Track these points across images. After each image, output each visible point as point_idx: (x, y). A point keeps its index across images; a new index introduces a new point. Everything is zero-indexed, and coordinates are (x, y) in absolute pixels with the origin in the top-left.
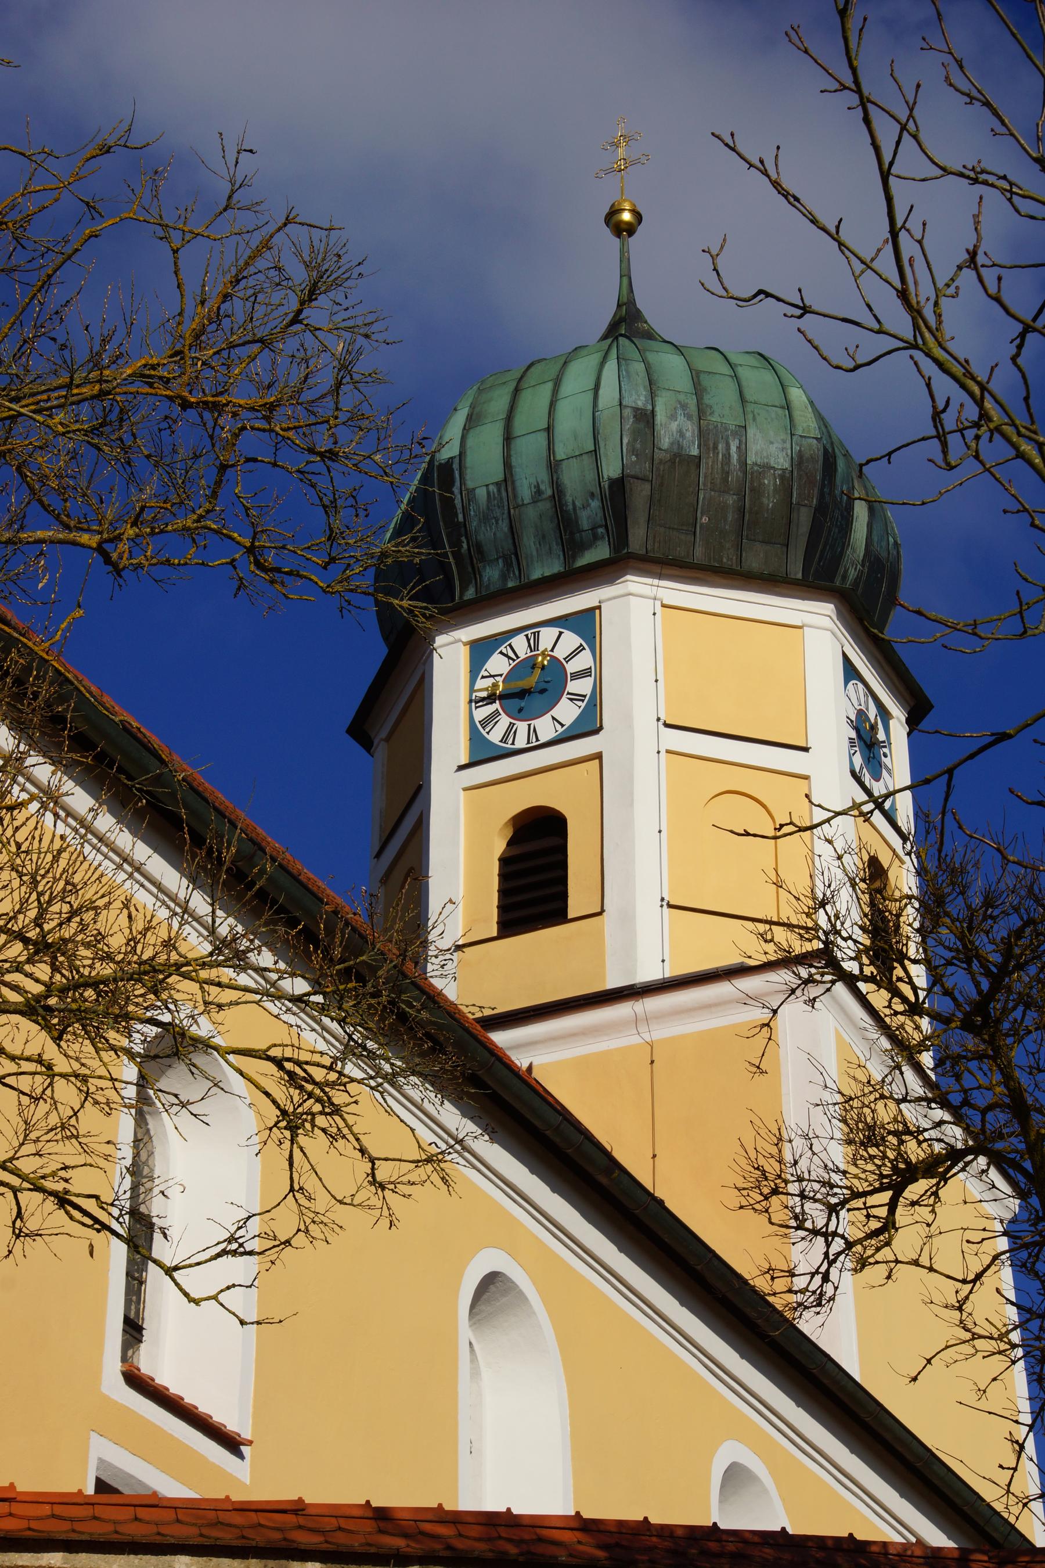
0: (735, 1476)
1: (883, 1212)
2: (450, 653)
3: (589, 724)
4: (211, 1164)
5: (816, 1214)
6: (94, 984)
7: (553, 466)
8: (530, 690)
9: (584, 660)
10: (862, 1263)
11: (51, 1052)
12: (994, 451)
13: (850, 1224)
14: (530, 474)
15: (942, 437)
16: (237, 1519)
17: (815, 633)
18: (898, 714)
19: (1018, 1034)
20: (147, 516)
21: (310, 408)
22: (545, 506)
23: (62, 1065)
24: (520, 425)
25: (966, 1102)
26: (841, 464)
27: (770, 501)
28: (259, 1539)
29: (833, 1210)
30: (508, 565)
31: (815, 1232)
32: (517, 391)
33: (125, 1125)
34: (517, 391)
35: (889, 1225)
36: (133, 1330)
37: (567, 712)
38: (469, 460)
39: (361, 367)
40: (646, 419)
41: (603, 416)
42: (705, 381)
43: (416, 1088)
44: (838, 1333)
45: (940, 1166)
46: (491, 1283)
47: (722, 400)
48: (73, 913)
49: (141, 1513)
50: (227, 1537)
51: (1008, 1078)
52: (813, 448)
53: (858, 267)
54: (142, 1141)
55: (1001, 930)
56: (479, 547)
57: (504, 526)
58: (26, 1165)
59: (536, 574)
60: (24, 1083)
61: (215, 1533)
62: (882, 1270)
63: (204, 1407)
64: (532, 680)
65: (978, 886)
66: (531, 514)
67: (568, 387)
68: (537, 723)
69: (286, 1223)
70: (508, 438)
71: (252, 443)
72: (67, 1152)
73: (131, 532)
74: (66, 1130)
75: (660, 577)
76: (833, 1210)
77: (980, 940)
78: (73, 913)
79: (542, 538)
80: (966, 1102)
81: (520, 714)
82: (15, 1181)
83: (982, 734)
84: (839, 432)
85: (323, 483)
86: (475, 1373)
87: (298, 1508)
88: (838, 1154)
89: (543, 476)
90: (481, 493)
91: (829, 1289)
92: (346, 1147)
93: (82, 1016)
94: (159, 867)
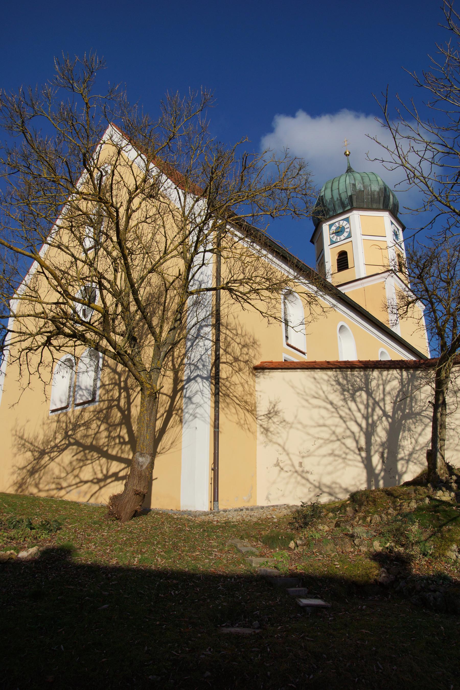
0: (382, 353)
1: (406, 309)
2: (325, 227)
3: (349, 236)
4: (296, 311)
5: (395, 311)
6: (276, 284)
7: (340, 194)
8: (339, 232)
9: (348, 226)
10: (402, 318)
11: (271, 296)
12: (417, 181)
13: (401, 312)
14: (336, 196)
15: (409, 179)
16: (306, 364)
17: (386, 216)
18: (400, 229)
19: (426, 279)
20: (277, 208)
21: (301, 187)
22: (339, 201)
23: (272, 297)
24: (333, 189)
25: (418, 291)
26: (387, 189)
27: (376, 196)
28: (310, 367)
29: (397, 310)
30: (334, 211)
31: (395, 314)
32: (332, 183)
33: (282, 305)
34: (332, 183)
35: (407, 311)
36: (287, 337)
37: (346, 234)
38: (326, 195)
39: (309, 180)
40: (354, 185)
41: (347, 186)
42: (363, 178)
43: (327, 297)
44: (397, 330)
45: (414, 302)
46: (342, 327)
47: (366, 180)
48: (272, 273)
49: (292, 364)
50: (305, 367)
51: (425, 286)
52: (382, 187)
53: (391, 153)
54: (285, 308)
55: (422, 262)
56: (329, 209)
57: (333, 205)
58: (269, 313)
59: (338, 212)
60: (267, 301)
61: (303, 366)
62: (406, 319)
63: (299, 349)
64: (339, 230)
65: (418, 255)
66: (337, 202)
67: (341, 181)
68: (341, 237)
69: (310, 319)
70: (332, 191)
71: (292, 195)
72: (275, 311)
73: (275, 211)
74: (274, 307)
75: (359, 210)
76: (397, 310)
77: (419, 264)
78: (272, 273)
79: (339, 206)
80: (418, 291)
81: (338, 236)
82: (268, 316)
83: (418, 229)
84: (387, 184)
85: (305, 199)
86: (340, 341)
87: (315, 362)
88: (398, 301)
89: (338, 196)
90: (328, 200)
91: (397, 322)
92: (319, 306)
93: (276, 289)
94: (284, 266)
